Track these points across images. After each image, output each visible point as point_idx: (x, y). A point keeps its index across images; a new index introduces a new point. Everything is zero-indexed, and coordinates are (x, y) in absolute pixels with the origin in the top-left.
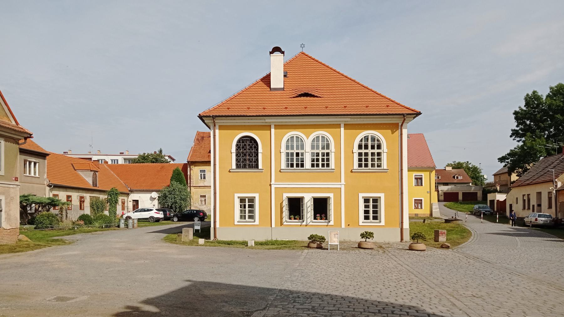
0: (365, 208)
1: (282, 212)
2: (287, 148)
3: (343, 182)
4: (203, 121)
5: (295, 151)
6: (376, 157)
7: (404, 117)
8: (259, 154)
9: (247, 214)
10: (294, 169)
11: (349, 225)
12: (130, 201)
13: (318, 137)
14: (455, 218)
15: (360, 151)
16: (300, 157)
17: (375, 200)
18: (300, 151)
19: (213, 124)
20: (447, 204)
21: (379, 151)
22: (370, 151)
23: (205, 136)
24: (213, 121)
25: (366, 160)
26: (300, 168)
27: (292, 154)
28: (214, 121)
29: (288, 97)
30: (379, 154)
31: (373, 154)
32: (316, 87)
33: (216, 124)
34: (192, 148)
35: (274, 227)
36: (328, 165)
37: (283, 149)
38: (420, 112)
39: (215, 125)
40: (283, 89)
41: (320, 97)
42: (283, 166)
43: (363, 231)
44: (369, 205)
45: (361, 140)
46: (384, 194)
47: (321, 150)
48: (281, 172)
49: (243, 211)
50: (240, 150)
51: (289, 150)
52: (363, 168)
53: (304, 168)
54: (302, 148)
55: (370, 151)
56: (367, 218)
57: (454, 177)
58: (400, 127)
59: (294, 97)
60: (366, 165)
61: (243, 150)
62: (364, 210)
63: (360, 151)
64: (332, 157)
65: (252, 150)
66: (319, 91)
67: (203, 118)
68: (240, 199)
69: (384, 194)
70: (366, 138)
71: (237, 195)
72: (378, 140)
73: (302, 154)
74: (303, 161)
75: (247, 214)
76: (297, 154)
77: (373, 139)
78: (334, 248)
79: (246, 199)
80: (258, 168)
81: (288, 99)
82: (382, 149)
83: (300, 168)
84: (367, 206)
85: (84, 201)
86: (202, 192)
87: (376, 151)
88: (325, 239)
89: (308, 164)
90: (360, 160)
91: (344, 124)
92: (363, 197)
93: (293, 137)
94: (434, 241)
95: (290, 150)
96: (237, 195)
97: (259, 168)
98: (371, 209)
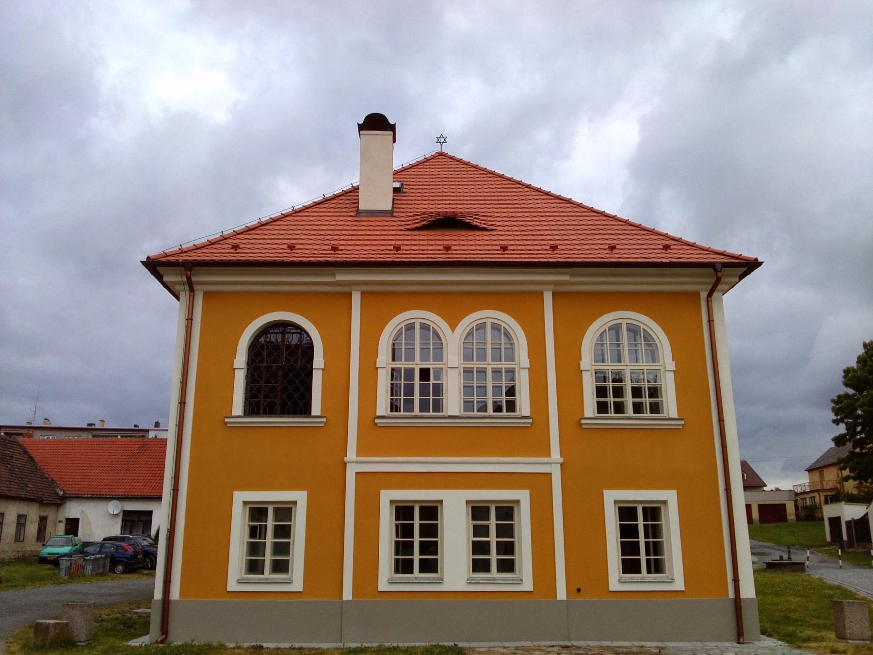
0: (474, 536)
1: (469, 553)
2: (600, 357)
3: (556, 454)
4: (160, 278)
5: (417, 365)
7: (716, 271)
8: (314, 372)
9: (417, 557)
10: (416, 417)
11: (579, 590)
12: (60, 522)
13: (410, 327)
14: (789, 558)
16: (432, 381)
17: (506, 511)
18: (431, 365)
19: (187, 287)
24: (185, 279)
26: (431, 413)
27: (409, 373)
28: (189, 278)
33: (196, 287)
35: (350, 598)
36: (438, 407)
37: (383, 358)
38: (756, 260)
39: (192, 290)
40: (391, 213)
42: (382, 407)
44: (488, 526)
45: (398, 335)
46: (383, 492)
47: (490, 362)
48: (581, 425)
49: (403, 548)
50: (262, 362)
51: (430, 361)
53: (517, 413)
54: (439, 357)
60: (619, 408)
61: (269, 361)
62: (473, 542)
65: (296, 361)
67: (157, 268)
68: (472, 507)
69: (383, 492)
71: (240, 497)
73: (439, 372)
74: (513, 394)
75: (417, 557)
76: (425, 374)
79: (267, 509)
80: (310, 413)
81: (402, 233)
82: (661, 363)
83: (431, 413)
84: (254, 532)
85: (24, 525)
87: (475, 365)
91: (553, 294)
92: (392, 502)
94: (838, 637)
95: (403, 362)
97: (313, 414)
98: (493, 539)
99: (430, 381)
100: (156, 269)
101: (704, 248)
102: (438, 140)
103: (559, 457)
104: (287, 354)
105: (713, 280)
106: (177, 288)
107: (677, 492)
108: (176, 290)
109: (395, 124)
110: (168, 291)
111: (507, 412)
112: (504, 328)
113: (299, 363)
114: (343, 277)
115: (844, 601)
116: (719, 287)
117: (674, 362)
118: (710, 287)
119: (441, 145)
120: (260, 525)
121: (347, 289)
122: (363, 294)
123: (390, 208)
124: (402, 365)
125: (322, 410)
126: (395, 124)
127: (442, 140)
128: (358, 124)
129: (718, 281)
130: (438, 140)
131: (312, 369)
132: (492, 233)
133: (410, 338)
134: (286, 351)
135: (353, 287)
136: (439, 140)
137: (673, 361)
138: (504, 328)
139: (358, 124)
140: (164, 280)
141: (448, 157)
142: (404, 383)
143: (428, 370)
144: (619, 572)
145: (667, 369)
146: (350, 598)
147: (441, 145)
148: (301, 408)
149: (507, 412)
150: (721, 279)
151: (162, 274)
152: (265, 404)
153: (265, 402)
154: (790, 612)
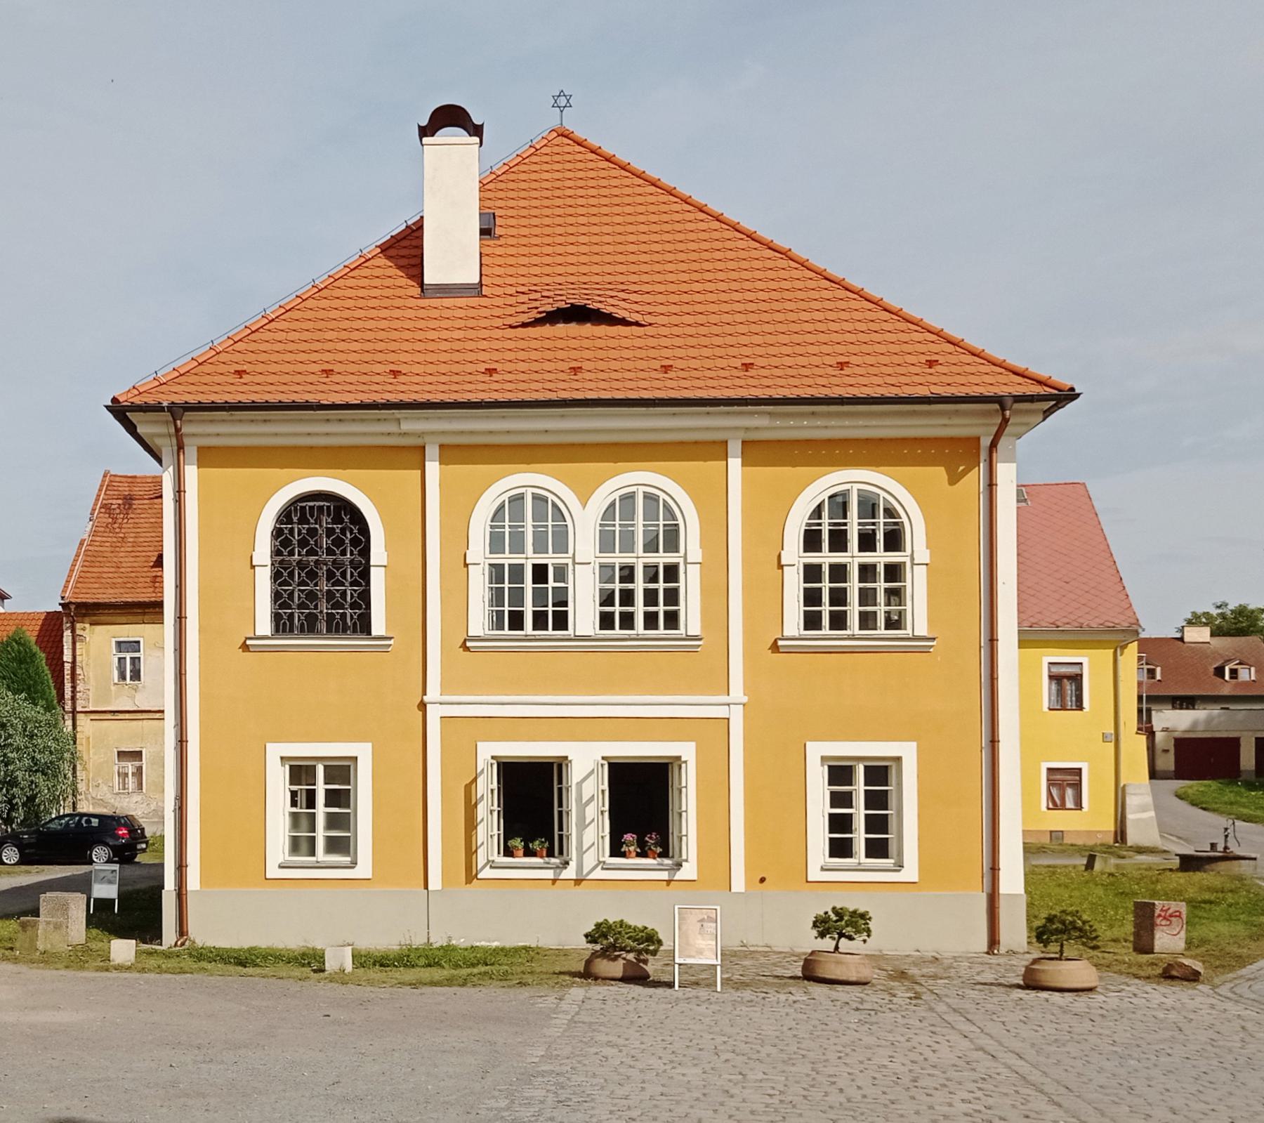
3: (737, 691)
4: (131, 428)
5: (529, 559)
6: (881, 585)
7: (1003, 409)
11: (762, 880)
15: (813, 558)
16: (551, 583)
17: (879, 773)
18: (550, 559)
20: (1191, 787)
21: (894, 557)
22: (853, 557)
23: (137, 491)
24: (172, 430)
25: (839, 597)
26: (550, 632)
27: (517, 571)
28: (177, 430)
29: (499, 322)
30: (894, 572)
31: (867, 572)
32: (621, 278)
33: (186, 441)
34: (81, 543)
36: (672, 620)
37: (479, 551)
38: (1072, 389)
39: (181, 447)
40: (477, 289)
41: (637, 324)
42: (479, 622)
43: (823, 907)
45: (817, 512)
47: (641, 553)
52: (826, 631)
55: (853, 557)
56: (840, 849)
57: (1219, 672)
58: (983, 455)
59: (524, 325)
63: (813, 558)
64: (691, 586)
66: (634, 297)
67: (127, 414)
70: (839, 504)
71: (276, 751)
72: (890, 512)
73: (561, 573)
76: (540, 573)
77: (869, 507)
78: (698, 979)
80: (369, 633)
81: (498, 333)
83: (661, 631)
86: (123, 734)
88: (660, 942)
89: (584, 616)
90: (812, 597)
93: (521, 497)
94: (1135, 949)
95: (507, 554)
96: (276, 751)
97: (374, 632)
98: (859, 812)
99: (547, 583)
100: (127, 416)
101: (995, 361)
102: (556, 102)
103: (742, 694)
104: (329, 542)
105: (999, 420)
106: (158, 442)
107: (918, 747)
108: (156, 445)
109: (482, 125)
110: (136, 440)
111: (510, 629)
112: (664, 500)
113: (348, 556)
114: (413, 424)
115: (1156, 902)
116: (1008, 430)
117: (928, 551)
118: (995, 429)
119: (562, 111)
120: (301, 789)
121: (419, 442)
122: (442, 446)
123: (477, 280)
124: (507, 559)
125: (703, 627)
126: (482, 125)
127: (563, 101)
128: (419, 126)
129: (1005, 421)
130: (556, 102)
131: (370, 566)
132: (649, 330)
133: (518, 515)
134: (328, 537)
135: (427, 439)
136: (558, 101)
137: (927, 548)
138: (664, 500)
139: (419, 126)
140: (138, 431)
141: (574, 142)
142: (553, 611)
143: (546, 566)
144: (824, 855)
145: (915, 562)
146: (439, 887)
147: (562, 111)
148: (285, 623)
149: (510, 629)
150: (1008, 420)
151: (135, 423)
152: (302, 618)
153: (302, 613)
154: (1068, 914)
